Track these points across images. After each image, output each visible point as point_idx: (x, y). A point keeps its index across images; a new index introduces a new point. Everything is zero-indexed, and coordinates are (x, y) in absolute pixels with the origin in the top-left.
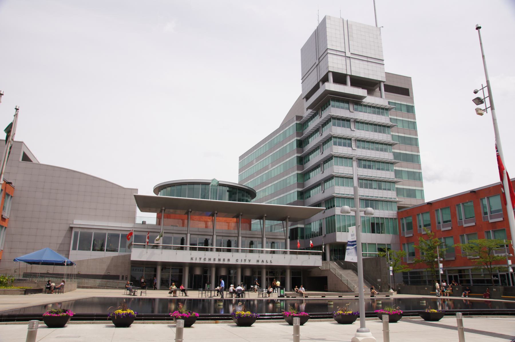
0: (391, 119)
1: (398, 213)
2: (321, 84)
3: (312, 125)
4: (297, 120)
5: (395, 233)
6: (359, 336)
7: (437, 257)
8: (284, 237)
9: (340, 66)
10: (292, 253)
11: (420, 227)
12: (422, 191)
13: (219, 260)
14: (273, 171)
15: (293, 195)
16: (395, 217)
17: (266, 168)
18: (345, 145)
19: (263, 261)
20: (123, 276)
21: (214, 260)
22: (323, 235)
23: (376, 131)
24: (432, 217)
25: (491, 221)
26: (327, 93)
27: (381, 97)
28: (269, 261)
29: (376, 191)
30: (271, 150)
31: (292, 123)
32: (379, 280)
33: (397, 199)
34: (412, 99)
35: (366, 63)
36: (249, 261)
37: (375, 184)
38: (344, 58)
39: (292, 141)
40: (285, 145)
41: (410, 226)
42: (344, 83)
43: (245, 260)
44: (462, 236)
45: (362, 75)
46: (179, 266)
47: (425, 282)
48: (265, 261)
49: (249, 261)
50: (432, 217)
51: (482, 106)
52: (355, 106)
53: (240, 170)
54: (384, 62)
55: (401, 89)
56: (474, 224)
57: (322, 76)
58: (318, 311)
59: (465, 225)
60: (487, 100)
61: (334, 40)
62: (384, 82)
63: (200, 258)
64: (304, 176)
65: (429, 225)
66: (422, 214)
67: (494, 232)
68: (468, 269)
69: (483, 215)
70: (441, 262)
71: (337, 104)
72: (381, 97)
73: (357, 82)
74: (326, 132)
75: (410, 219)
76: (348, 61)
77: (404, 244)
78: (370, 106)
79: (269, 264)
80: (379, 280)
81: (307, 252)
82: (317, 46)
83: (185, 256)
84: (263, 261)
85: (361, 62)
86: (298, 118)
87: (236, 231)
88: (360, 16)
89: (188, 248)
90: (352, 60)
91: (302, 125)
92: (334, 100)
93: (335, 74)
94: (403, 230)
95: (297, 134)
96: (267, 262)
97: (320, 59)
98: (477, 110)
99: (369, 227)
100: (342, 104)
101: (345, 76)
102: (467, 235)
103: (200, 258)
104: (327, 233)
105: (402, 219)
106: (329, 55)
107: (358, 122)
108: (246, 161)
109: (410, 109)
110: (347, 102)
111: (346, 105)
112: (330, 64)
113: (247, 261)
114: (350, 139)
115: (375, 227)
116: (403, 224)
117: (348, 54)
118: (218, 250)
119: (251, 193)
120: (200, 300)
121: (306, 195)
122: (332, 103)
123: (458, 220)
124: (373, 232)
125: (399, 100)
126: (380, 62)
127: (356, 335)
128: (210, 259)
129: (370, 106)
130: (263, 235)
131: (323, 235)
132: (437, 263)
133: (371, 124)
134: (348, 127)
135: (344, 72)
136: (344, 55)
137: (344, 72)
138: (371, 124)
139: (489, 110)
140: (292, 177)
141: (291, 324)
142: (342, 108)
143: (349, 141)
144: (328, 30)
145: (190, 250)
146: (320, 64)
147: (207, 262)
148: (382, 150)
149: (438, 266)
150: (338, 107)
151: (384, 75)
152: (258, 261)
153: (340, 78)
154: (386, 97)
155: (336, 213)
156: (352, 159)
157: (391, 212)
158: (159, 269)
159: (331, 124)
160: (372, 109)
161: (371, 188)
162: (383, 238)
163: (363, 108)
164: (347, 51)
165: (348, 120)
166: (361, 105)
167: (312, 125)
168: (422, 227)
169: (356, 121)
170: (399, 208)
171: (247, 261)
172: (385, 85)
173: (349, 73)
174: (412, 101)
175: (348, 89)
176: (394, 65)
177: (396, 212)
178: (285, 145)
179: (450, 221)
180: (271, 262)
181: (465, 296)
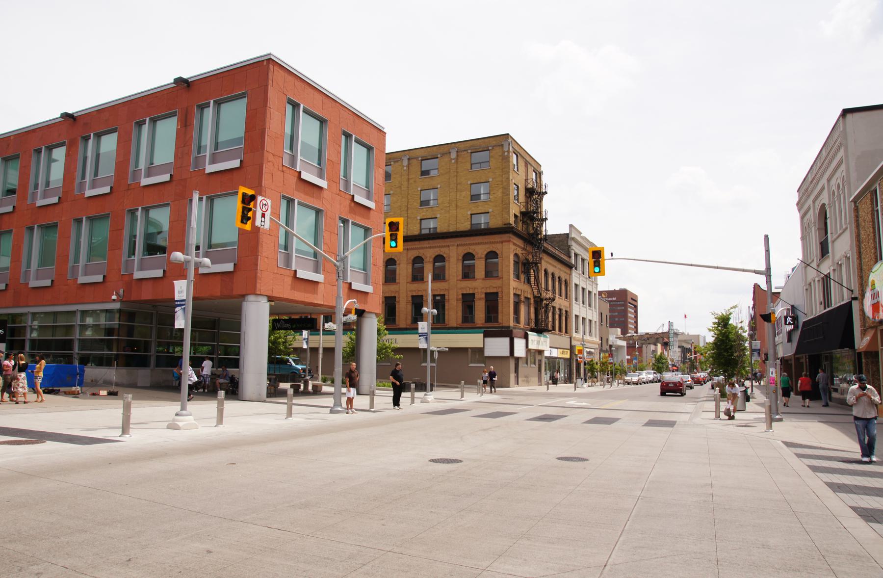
23: (306, 194)
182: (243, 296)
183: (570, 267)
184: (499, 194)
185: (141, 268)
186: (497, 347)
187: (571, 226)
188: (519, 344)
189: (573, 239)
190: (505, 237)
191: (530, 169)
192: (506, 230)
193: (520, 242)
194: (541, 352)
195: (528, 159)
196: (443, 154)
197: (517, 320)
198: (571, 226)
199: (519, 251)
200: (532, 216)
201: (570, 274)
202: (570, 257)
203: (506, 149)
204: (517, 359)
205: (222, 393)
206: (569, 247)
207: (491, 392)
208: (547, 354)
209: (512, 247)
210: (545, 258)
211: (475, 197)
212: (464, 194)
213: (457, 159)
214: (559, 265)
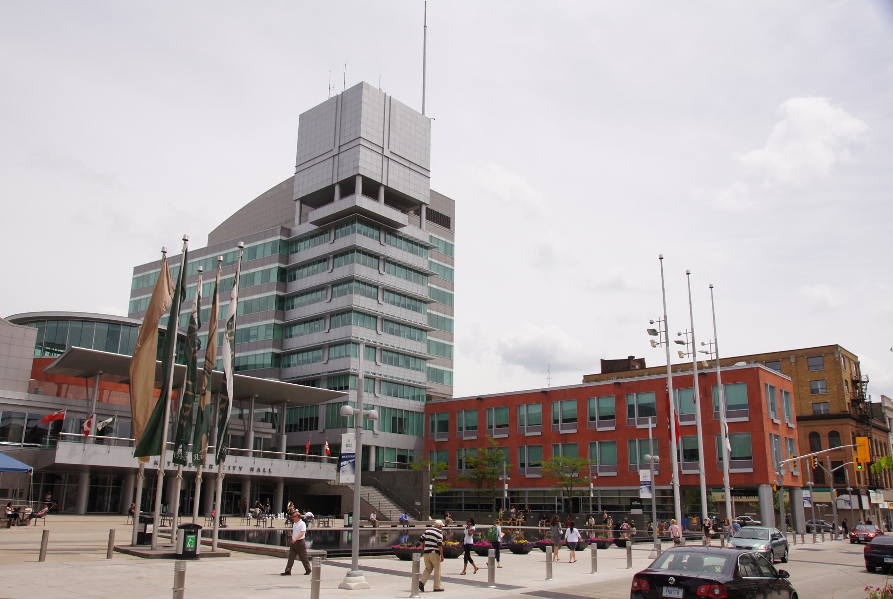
0: (430, 262)
1: (426, 405)
5: (419, 434)
6: (351, 582)
8: (243, 428)
9: (374, 170)
10: (287, 457)
11: (461, 429)
12: (451, 373)
16: (422, 411)
19: (259, 470)
20: (14, 491)
23: (409, 279)
24: (482, 418)
25: (562, 432)
26: (357, 210)
29: (402, 369)
31: (272, 236)
32: (418, 503)
33: (427, 385)
34: (453, 233)
35: (407, 170)
36: (240, 468)
37: (401, 359)
38: (380, 157)
39: (267, 267)
41: (444, 426)
43: (234, 467)
44: (522, 448)
45: (401, 190)
47: (460, 506)
48: (262, 470)
49: (240, 468)
50: (482, 418)
51: (656, 339)
52: (388, 237)
54: (431, 175)
55: (442, 219)
56: (539, 433)
58: (332, 545)
59: (527, 434)
60: (663, 334)
61: (370, 127)
64: (284, 329)
68: (524, 492)
69: (552, 424)
70: (507, 482)
71: (365, 228)
73: (396, 200)
75: (445, 417)
76: (385, 163)
77: (432, 452)
78: (406, 240)
79: (267, 474)
80: (418, 503)
81: (315, 458)
82: (334, 122)
84: (259, 470)
85: (402, 168)
88: (407, 96)
89: (284, 457)
90: (391, 162)
91: (289, 245)
92: (362, 221)
93: (367, 182)
94: (433, 430)
96: (264, 471)
97: (342, 149)
98: (652, 342)
99: (388, 423)
100: (371, 231)
101: (379, 185)
103: (234, 467)
104: (327, 428)
106: (362, 149)
107: (389, 262)
108: (146, 279)
109: (449, 250)
110: (378, 228)
111: (376, 233)
112: (361, 164)
114: (377, 287)
115: (397, 423)
116: (433, 423)
118: (255, 455)
120: (243, 531)
121: (284, 361)
122: (358, 226)
123: (519, 426)
124: (394, 431)
125: (443, 236)
126: (424, 172)
127: (345, 581)
129: (406, 240)
131: (320, 430)
132: (501, 484)
133: (405, 268)
138: (405, 268)
139: (664, 345)
141: (544, 551)
142: (371, 236)
143: (375, 290)
144: (364, 106)
145: (286, 458)
146: (341, 155)
147: (237, 472)
148: (409, 307)
149: (503, 487)
150: (365, 234)
151: (428, 194)
153: (371, 189)
156: (376, 317)
157: (418, 403)
160: (409, 244)
161: (397, 365)
162: (406, 441)
163: (399, 241)
164: (386, 147)
165: (375, 256)
166: (396, 236)
168: (464, 429)
169: (387, 260)
173: (385, 183)
174: (452, 236)
176: (442, 181)
177: (423, 404)
179: (507, 426)
180: (270, 471)
181: (542, 526)
182: (759, 485)
183: (887, 431)
184: (835, 388)
185: (466, 436)
186: (845, 502)
187: (883, 397)
188: (864, 499)
189: (887, 407)
190: (844, 421)
191: (852, 363)
192: (842, 416)
193: (853, 423)
194: (877, 505)
195: (850, 357)
196: (783, 359)
197: (859, 482)
198: (883, 397)
199: (854, 430)
200: (858, 400)
201: (888, 437)
202: (885, 423)
203: (836, 356)
204: (864, 511)
205: (814, 531)
206: (884, 414)
207: (832, 539)
208: (881, 506)
209: (850, 427)
210: (873, 430)
211: (814, 391)
212: (804, 388)
213: (796, 363)
214: (879, 433)
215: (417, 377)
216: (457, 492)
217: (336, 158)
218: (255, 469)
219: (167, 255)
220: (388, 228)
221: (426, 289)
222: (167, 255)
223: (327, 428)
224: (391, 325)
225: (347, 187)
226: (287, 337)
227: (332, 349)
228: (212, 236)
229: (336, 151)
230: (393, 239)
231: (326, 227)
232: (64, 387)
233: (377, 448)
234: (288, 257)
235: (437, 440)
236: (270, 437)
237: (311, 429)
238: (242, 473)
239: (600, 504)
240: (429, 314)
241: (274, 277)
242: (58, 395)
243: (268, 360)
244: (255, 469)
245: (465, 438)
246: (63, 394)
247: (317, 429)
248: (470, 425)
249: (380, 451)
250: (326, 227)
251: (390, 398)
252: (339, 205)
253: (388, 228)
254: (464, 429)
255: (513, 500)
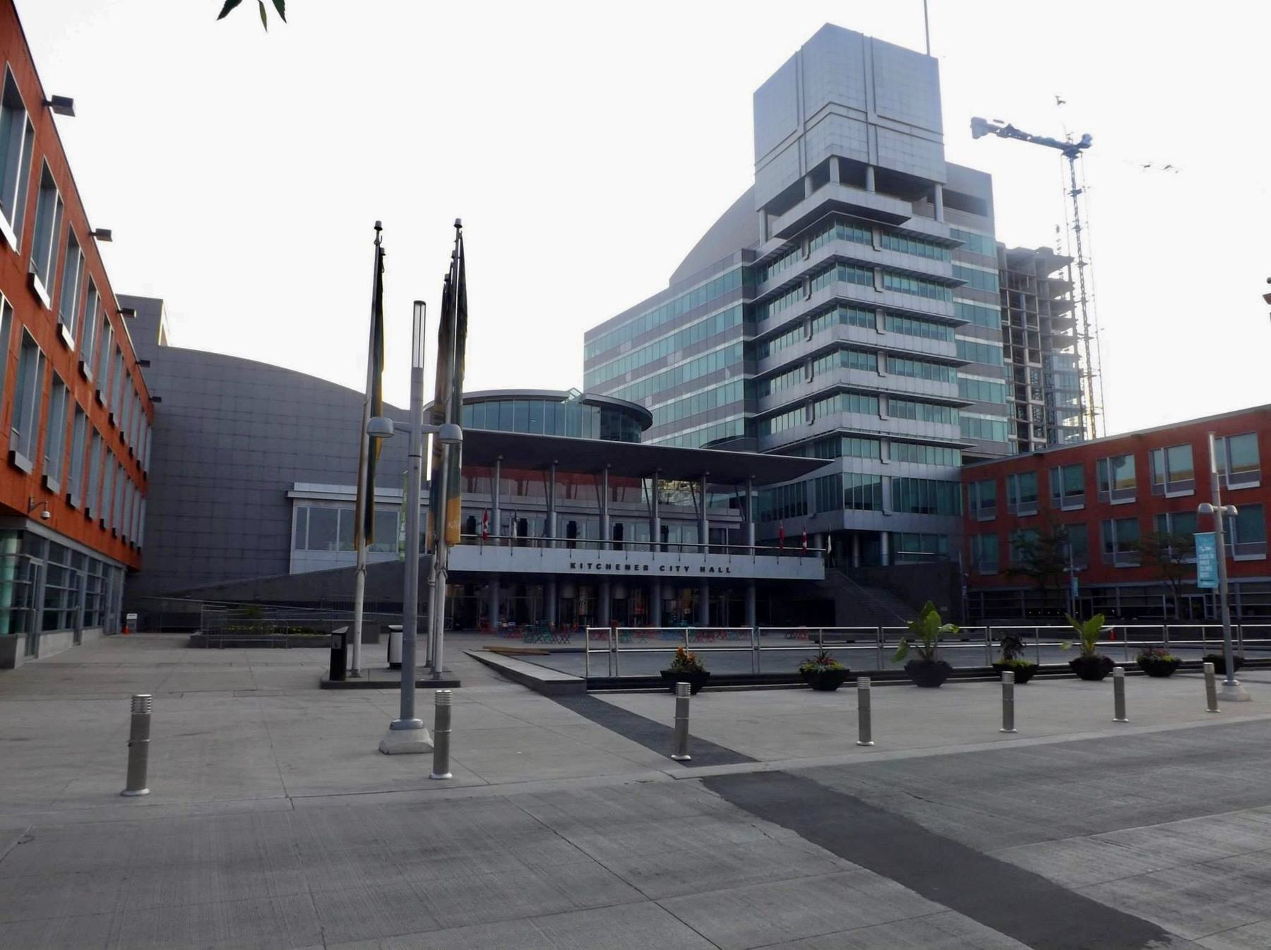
2: (808, 184)
3: (780, 275)
4: (743, 259)
7: (1068, 566)
11: (1014, 501)
13: (628, 567)
14: (686, 369)
15: (735, 424)
17: (662, 362)
18: (863, 324)
21: (618, 567)
22: (810, 515)
24: (1043, 483)
27: (936, 219)
28: (724, 569)
30: (674, 323)
36: (687, 568)
39: (730, 306)
40: (714, 314)
42: (860, 183)
43: (678, 568)
45: (900, 168)
46: (739, 585)
48: (716, 570)
49: (687, 568)
53: (588, 364)
57: (814, 164)
62: (942, 184)
63: (590, 565)
65: (1033, 498)
66: (1020, 475)
67: (1173, 516)
72: (936, 219)
73: (892, 183)
74: (822, 293)
83: (553, 560)
84: (712, 570)
86: (748, 254)
87: (542, 501)
90: (880, 131)
91: (756, 270)
92: (843, 221)
93: (844, 162)
95: (744, 289)
100: (858, 233)
101: (867, 165)
102: (1117, 521)
103: (590, 565)
104: (819, 511)
105: (972, 483)
108: (602, 343)
110: (869, 227)
111: (867, 235)
113: (682, 569)
117: (872, 118)
119: (641, 418)
128: (608, 567)
130: (549, 506)
131: (810, 515)
134: (868, 285)
135: (863, 159)
136: (862, 117)
137: (863, 159)
140: (733, 387)
142: (860, 241)
149: (1069, 583)
152: (703, 569)
153: (853, 173)
154: (948, 219)
155: (845, 470)
158: (753, 591)
159: (835, 271)
167: (780, 275)
168: (1018, 503)
170: (965, 460)
171: (682, 569)
172: (945, 192)
173: (873, 162)
175: (870, 199)
178: (714, 314)
179: (1079, 492)
215: (946, 430)
216: (1013, 592)
217: (802, 140)
218: (707, 570)
219: (101, 245)
220: (887, 225)
221: (950, 306)
222: (101, 245)
223: (819, 511)
224: (899, 362)
225: (820, 176)
226: (762, 396)
227: (817, 405)
228: (672, 280)
229: (801, 132)
230: (894, 240)
231: (799, 237)
232: (525, 483)
233: (890, 534)
234: (756, 289)
235: (980, 519)
236: (737, 527)
237: (799, 514)
238: (689, 574)
239: (1239, 604)
240: (957, 341)
241: (739, 319)
242: (569, 496)
243: (740, 430)
244: (707, 570)
245: (1020, 514)
246: (619, 498)
247: (806, 513)
248: (1027, 494)
249: (896, 537)
250: (799, 237)
251: (905, 464)
252: (813, 201)
253: (887, 225)
254: (1018, 503)
255: (1097, 602)
